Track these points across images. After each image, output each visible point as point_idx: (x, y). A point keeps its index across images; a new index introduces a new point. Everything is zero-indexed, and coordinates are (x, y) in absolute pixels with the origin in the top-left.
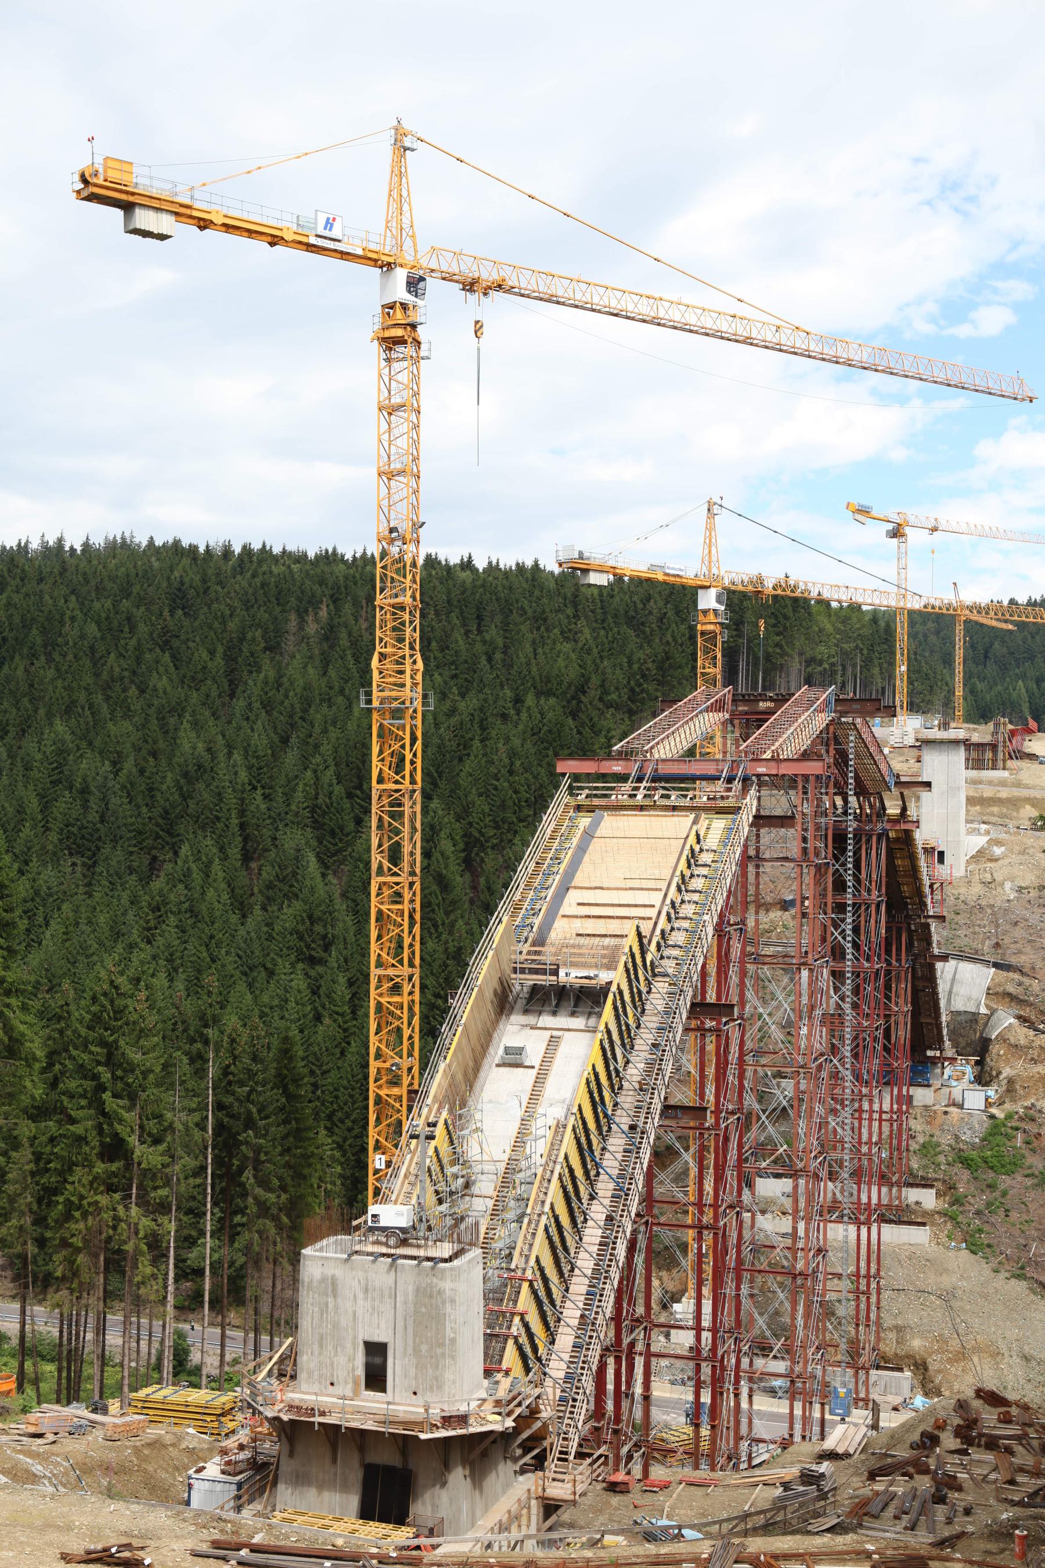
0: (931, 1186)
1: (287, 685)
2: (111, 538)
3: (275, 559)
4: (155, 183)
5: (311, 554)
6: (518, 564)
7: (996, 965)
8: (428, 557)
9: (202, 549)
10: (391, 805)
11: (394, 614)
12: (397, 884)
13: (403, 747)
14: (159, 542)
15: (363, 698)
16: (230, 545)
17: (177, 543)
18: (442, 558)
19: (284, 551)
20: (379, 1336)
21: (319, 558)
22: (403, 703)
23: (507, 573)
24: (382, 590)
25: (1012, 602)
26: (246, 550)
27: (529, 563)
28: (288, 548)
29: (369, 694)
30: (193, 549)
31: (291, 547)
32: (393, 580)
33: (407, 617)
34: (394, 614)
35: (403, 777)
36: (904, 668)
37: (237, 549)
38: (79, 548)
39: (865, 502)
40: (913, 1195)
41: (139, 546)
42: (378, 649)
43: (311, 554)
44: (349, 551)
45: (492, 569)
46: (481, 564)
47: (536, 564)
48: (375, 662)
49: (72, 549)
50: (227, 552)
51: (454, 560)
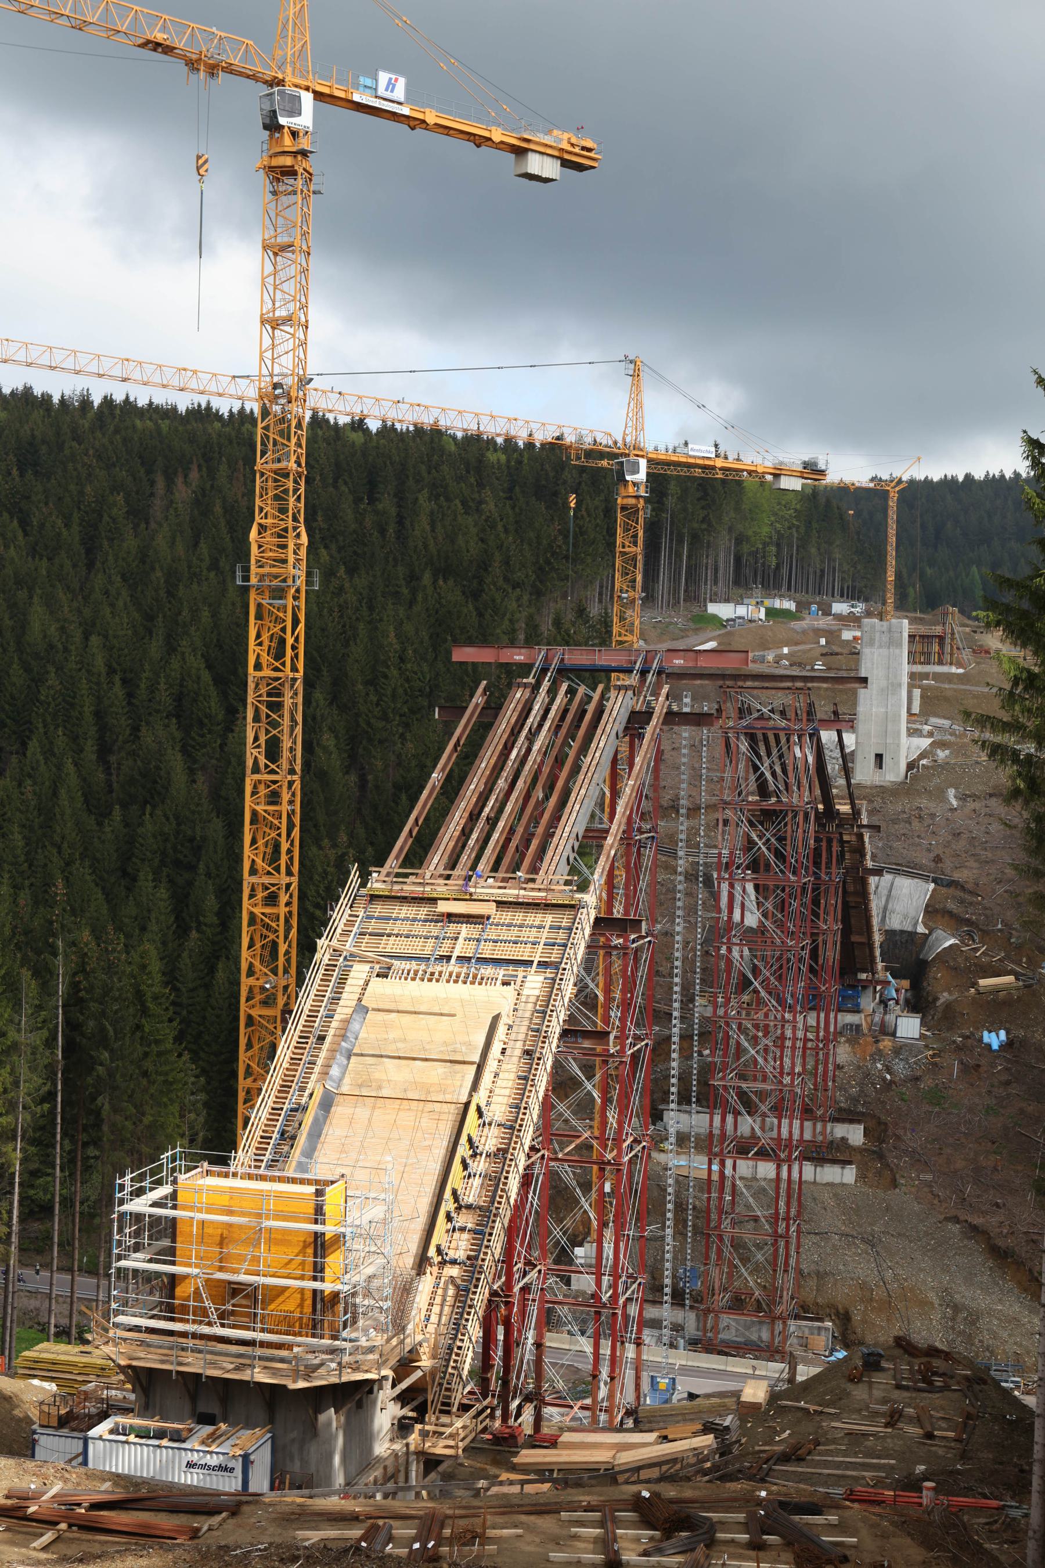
0: (859, 1122)
7: (934, 881)
15: (239, 574)
16: (89, 395)
25: (968, 477)
29: (246, 569)
30: (46, 398)
35: (283, 664)
37: (97, 400)
40: (840, 1130)
44: (224, 406)
45: (388, 431)
50: (85, 402)
51: (343, 420)
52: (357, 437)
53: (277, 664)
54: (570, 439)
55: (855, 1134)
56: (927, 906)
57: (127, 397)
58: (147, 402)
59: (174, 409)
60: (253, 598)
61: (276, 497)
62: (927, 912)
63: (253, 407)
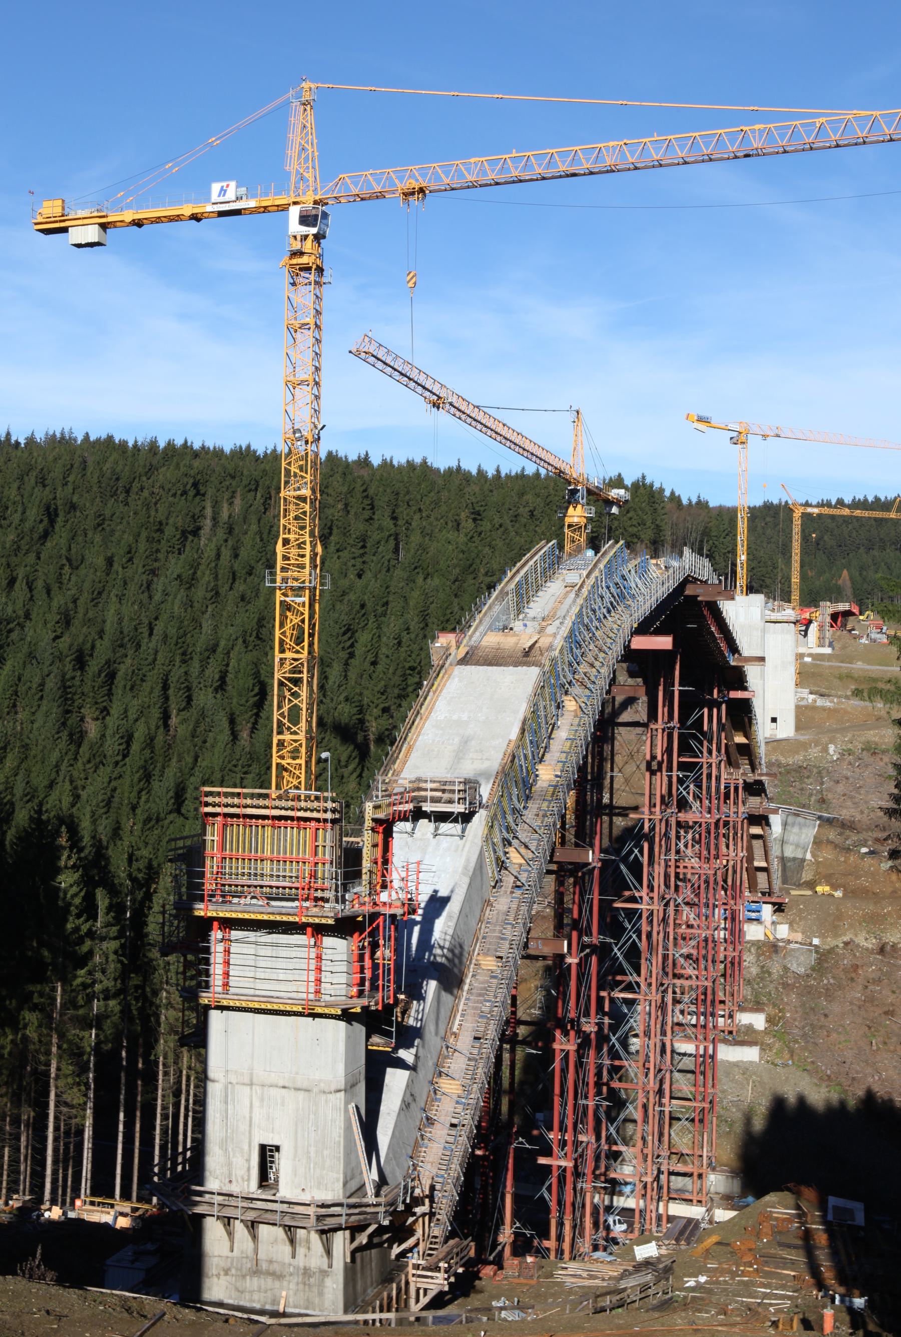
1: (423, 656)
2: (51, 433)
3: (196, 455)
4: (454, 1174)
5: (227, 450)
6: (408, 461)
8: (330, 454)
9: (131, 444)
10: (291, 672)
11: (297, 505)
12: (295, 741)
13: (303, 621)
14: (93, 438)
15: (268, 577)
16: (156, 441)
17: (110, 438)
18: (341, 454)
19: (203, 447)
20: (270, 1140)
21: (233, 452)
22: (304, 582)
23: (400, 468)
24: (287, 483)
26: (170, 445)
27: (418, 460)
28: (207, 444)
29: (273, 574)
30: (124, 444)
31: (210, 444)
32: (295, 475)
33: (307, 508)
34: (297, 505)
35: (303, 648)
36: (744, 557)
37: (162, 444)
38: (22, 441)
39: (704, 414)
41: (75, 440)
42: (282, 536)
43: (227, 450)
44: (261, 447)
45: (387, 465)
46: (376, 461)
47: (424, 462)
48: (279, 548)
49: (17, 443)
50: (153, 444)
51: (353, 457)
52: (364, 473)
53: (298, 648)
54: (40, 436)
55: (758, 1021)
56: (815, 837)
57: (186, 442)
58: (640, 476)
59: (222, 450)
60: (279, 597)
61: (296, 518)
62: (815, 843)
63: (282, 448)
